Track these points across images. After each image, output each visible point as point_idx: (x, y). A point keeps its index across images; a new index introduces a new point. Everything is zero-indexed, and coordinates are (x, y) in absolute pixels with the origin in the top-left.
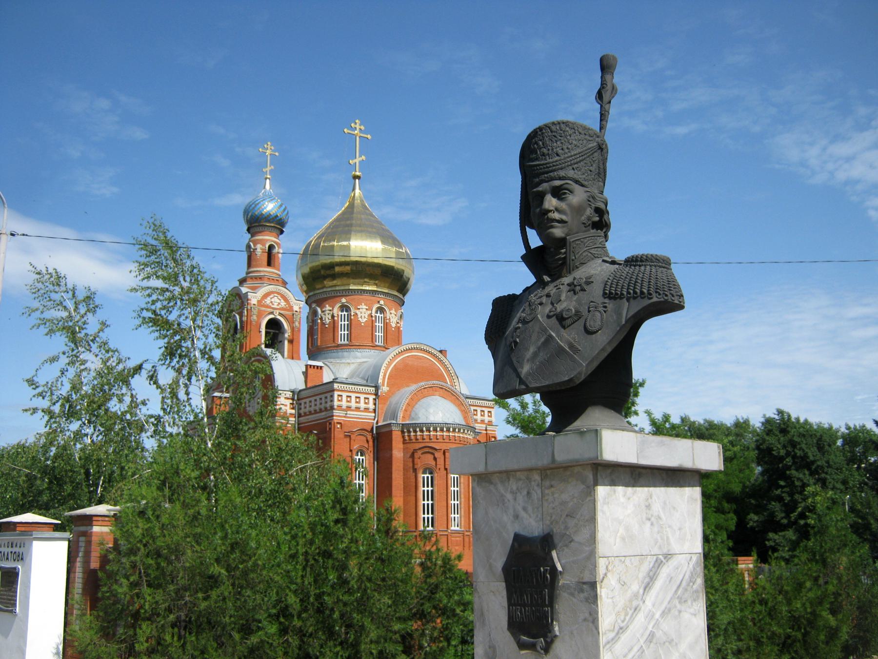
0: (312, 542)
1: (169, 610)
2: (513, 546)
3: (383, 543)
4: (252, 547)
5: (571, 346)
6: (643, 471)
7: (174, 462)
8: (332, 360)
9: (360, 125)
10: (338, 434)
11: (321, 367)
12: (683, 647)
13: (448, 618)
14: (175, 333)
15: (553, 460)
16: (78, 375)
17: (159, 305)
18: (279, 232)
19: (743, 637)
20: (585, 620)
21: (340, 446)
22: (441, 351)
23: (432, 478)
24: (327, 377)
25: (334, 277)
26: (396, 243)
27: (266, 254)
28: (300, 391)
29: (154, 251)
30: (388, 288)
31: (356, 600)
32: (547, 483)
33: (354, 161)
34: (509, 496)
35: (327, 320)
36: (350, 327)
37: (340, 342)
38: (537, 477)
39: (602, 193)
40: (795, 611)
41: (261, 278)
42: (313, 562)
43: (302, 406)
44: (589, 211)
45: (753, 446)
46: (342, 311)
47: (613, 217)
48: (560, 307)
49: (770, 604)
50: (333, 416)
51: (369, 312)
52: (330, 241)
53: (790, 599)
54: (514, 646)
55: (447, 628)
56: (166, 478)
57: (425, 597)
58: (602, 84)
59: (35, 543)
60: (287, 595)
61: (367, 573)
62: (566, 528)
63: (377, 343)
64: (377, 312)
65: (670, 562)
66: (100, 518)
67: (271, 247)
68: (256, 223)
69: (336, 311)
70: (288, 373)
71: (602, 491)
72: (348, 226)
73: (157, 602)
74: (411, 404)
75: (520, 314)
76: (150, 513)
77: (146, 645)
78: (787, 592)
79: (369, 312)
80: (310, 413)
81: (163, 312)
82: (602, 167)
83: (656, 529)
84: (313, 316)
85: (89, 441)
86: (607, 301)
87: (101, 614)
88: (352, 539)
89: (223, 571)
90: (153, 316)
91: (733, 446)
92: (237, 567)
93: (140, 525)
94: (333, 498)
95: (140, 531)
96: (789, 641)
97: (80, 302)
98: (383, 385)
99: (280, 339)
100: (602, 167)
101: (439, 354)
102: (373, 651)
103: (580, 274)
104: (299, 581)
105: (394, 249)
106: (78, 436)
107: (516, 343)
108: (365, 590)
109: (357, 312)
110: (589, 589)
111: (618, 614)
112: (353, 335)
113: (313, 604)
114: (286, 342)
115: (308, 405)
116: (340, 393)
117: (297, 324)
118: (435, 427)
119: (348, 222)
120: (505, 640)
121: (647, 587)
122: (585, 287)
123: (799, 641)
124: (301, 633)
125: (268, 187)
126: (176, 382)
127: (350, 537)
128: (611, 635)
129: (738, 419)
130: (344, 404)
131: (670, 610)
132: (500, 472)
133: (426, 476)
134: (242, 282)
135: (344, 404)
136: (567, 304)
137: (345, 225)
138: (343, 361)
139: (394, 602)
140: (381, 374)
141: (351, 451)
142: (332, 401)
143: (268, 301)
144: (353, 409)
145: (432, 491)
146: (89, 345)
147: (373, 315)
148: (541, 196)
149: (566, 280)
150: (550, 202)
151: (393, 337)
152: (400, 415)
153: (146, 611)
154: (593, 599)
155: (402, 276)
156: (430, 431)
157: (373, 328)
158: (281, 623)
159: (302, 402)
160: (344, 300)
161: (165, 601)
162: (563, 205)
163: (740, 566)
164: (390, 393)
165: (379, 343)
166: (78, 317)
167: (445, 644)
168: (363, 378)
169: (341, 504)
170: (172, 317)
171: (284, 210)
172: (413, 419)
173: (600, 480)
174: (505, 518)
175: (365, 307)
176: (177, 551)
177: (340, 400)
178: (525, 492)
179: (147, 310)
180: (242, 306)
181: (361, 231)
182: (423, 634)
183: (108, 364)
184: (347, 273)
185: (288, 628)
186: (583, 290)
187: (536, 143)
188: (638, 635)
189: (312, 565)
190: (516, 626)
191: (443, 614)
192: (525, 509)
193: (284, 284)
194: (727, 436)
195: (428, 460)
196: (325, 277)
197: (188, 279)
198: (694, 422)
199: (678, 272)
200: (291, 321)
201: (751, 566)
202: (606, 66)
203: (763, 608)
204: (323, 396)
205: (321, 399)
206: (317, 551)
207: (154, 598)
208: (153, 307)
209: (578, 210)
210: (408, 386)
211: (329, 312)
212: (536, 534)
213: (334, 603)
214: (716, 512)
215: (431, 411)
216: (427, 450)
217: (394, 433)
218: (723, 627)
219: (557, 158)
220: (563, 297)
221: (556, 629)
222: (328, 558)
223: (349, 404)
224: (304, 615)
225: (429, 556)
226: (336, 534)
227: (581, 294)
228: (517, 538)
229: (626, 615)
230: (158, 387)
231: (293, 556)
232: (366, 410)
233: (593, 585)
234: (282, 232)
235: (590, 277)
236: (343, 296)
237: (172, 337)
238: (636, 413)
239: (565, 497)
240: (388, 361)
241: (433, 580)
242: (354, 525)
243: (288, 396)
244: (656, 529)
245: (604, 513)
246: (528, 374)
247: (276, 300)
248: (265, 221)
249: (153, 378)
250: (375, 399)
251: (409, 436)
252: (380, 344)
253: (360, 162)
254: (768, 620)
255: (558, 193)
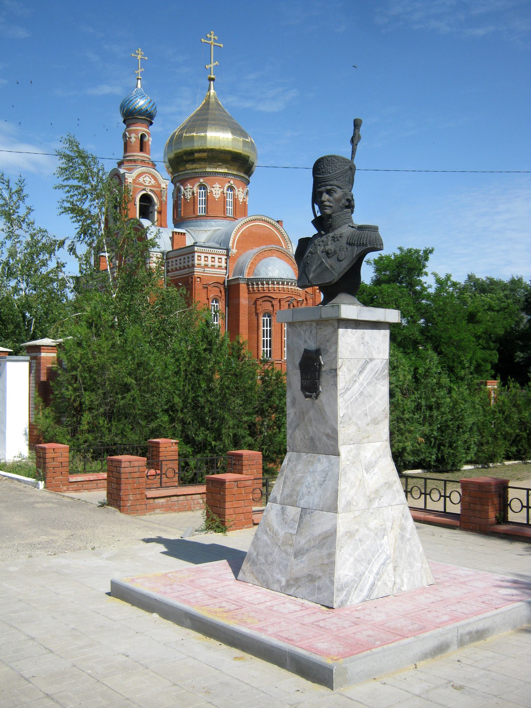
0: (189, 363)
1: (100, 405)
2: (303, 354)
3: (236, 364)
4: (151, 366)
5: (331, 266)
6: (361, 323)
7: (97, 310)
8: (192, 228)
9: (214, 36)
10: (198, 286)
11: (184, 234)
12: (377, 399)
13: (279, 413)
14: (87, 218)
15: (321, 317)
16: (14, 246)
17: (75, 198)
18: (149, 124)
19: (484, 434)
20: (332, 385)
21: (200, 295)
22: (278, 222)
23: (270, 319)
24: (189, 242)
25: (194, 161)
26: (244, 134)
27: (139, 142)
28: (168, 252)
29: (70, 159)
30: (237, 170)
31: (219, 401)
32: (319, 327)
33: (210, 66)
34: (302, 332)
35: (189, 196)
36: (206, 202)
37: (199, 214)
38: (314, 324)
39: (351, 191)
40: (524, 418)
41: (135, 161)
42: (190, 376)
43: (170, 264)
44: (344, 201)
45: (523, 299)
46: (201, 189)
47: (357, 203)
48: (327, 248)
49: (506, 413)
50: (194, 272)
51: (222, 190)
52: (191, 132)
53: (521, 410)
54: (303, 397)
55: (278, 420)
56: (93, 321)
57: (264, 400)
58: (354, 135)
59: (9, 364)
60: (174, 397)
61: (226, 383)
62: (326, 346)
63: (228, 215)
64: (228, 190)
65: (372, 363)
66: (46, 348)
67: (143, 136)
68: (131, 116)
69: (195, 189)
70: (162, 237)
71: (341, 331)
72: (204, 120)
73: (92, 401)
74: (254, 264)
75: (310, 249)
76: (84, 343)
77: (87, 426)
78: (519, 405)
79: (222, 190)
80: (176, 270)
81: (78, 203)
82: (351, 178)
83: (366, 348)
84: (177, 193)
85: (24, 293)
86: (348, 246)
87: (53, 409)
88: (215, 362)
89: (133, 381)
90: (71, 206)
91: (507, 299)
92: (142, 379)
93: (79, 351)
94: (202, 334)
95: (79, 355)
96: (518, 438)
97: (13, 193)
98: (233, 248)
99: (151, 210)
100: (351, 178)
101: (276, 224)
102: (231, 434)
103: (337, 232)
104: (181, 388)
105: (241, 139)
106: (16, 290)
107: (307, 263)
108: (225, 394)
109: (212, 189)
110: (334, 372)
111: (346, 383)
112: (209, 208)
113: (190, 403)
114: (156, 213)
115: (174, 263)
116: (199, 254)
117: (164, 198)
118: (273, 281)
119: (205, 117)
120: (299, 395)
121: (361, 372)
122: (339, 239)
123: (525, 439)
124: (183, 422)
125: (139, 86)
126: (89, 253)
127: (214, 360)
128: (343, 391)
129: (513, 277)
130: (203, 262)
131: (371, 383)
132: (299, 322)
133: (265, 318)
134: (120, 164)
135: (203, 262)
136: (331, 247)
137: (203, 119)
138: (202, 229)
139: (244, 402)
140: (231, 240)
141: (208, 299)
142: (193, 260)
143: (141, 180)
144: (210, 266)
145: (270, 330)
146: (21, 224)
147: (225, 192)
148: (321, 193)
149: (331, 234)
150: (325, 197)
151: (240, 210)
152: (246, 271)
153: (86, 406)
154: (336, 376)
155: (248, 161)
156: (269, 284)
157: (225, 203)
158: (170, 415)
159: (170, 261)
160: (202, 180)
161: (97, 400)
162: (331, 198)
163: (488, 387)
164: (238, 255)
165: (230, 214)
166: (12, 204)
167: (277, 430)
168: (217, 243)
169: (207, 338)
170: (85, 206)
171: (153, 105)
172: (256, 275)
173: (340, 326)
174: (301, 342)
175: (219, 186)
176: (103, 367)
177: (200, 260)
178: (309, 331)
179: (68, 202)
180: (121, 183)
181: (215, 125)
182: (262, 425)
183: (35, 238)
184: (204, 159)
185: (174, 419)
186: (338, 240)
187: (320, 166)
188: (355, 392)
189: (189, 378)
190: (304, 388)
191: (276, 411)
192: (309, 338)
193: (154, 166)
194: (504, 290)
195: (267, 306)
196: (187, 162)
197: (95, 179)
198: (478, 279)
199: (381, 232)
200: (160, 196)
201: (496, 387)
202: (357, 124)
203: (501, 415)
204: (186, 257)
205: (184, 259)
206: (193, 369)
207: (90, 398)
208: (71, 200)
209: (338, 201)
210: (252, 249)
211: (190, 190)
212: (313, 349)
213: (205, 402)
214: (481, 349)
215: (270, 268)
216: (266, 298)
217: (241, 285)
218: (469, 426)
219: (329, 175)
220: (329, 243)
221: (321, 389)
222: (200, 374)
223: (206, 263)
224: (185, 410)
225: (266, 373)
226: (205, 358)
227: (337, 242)
228: (306, 351)
229: (350, 383)
230: (77, 257)
231: (177, 373)
232: (220, 267)
233: (336, 370)
234: (151, 124)
235: (342, 234)
236: (201, 177)
237: (85, 220)
238: (426, 274)
239: (326, 333)
240: (237, 229)
241: (269, 389)
242: (216, 352)
243: (159, 256)
244: (366, 348)
245: (341, 340)
246: (312, 278)
247: (147, 179)
248: (138, 115)
249: (72, 250)
250: (226, 259)
251: (253, 288)
252: (230, 215)
253: (214, 67)
254: (503, 423)
255: (329, 192)
